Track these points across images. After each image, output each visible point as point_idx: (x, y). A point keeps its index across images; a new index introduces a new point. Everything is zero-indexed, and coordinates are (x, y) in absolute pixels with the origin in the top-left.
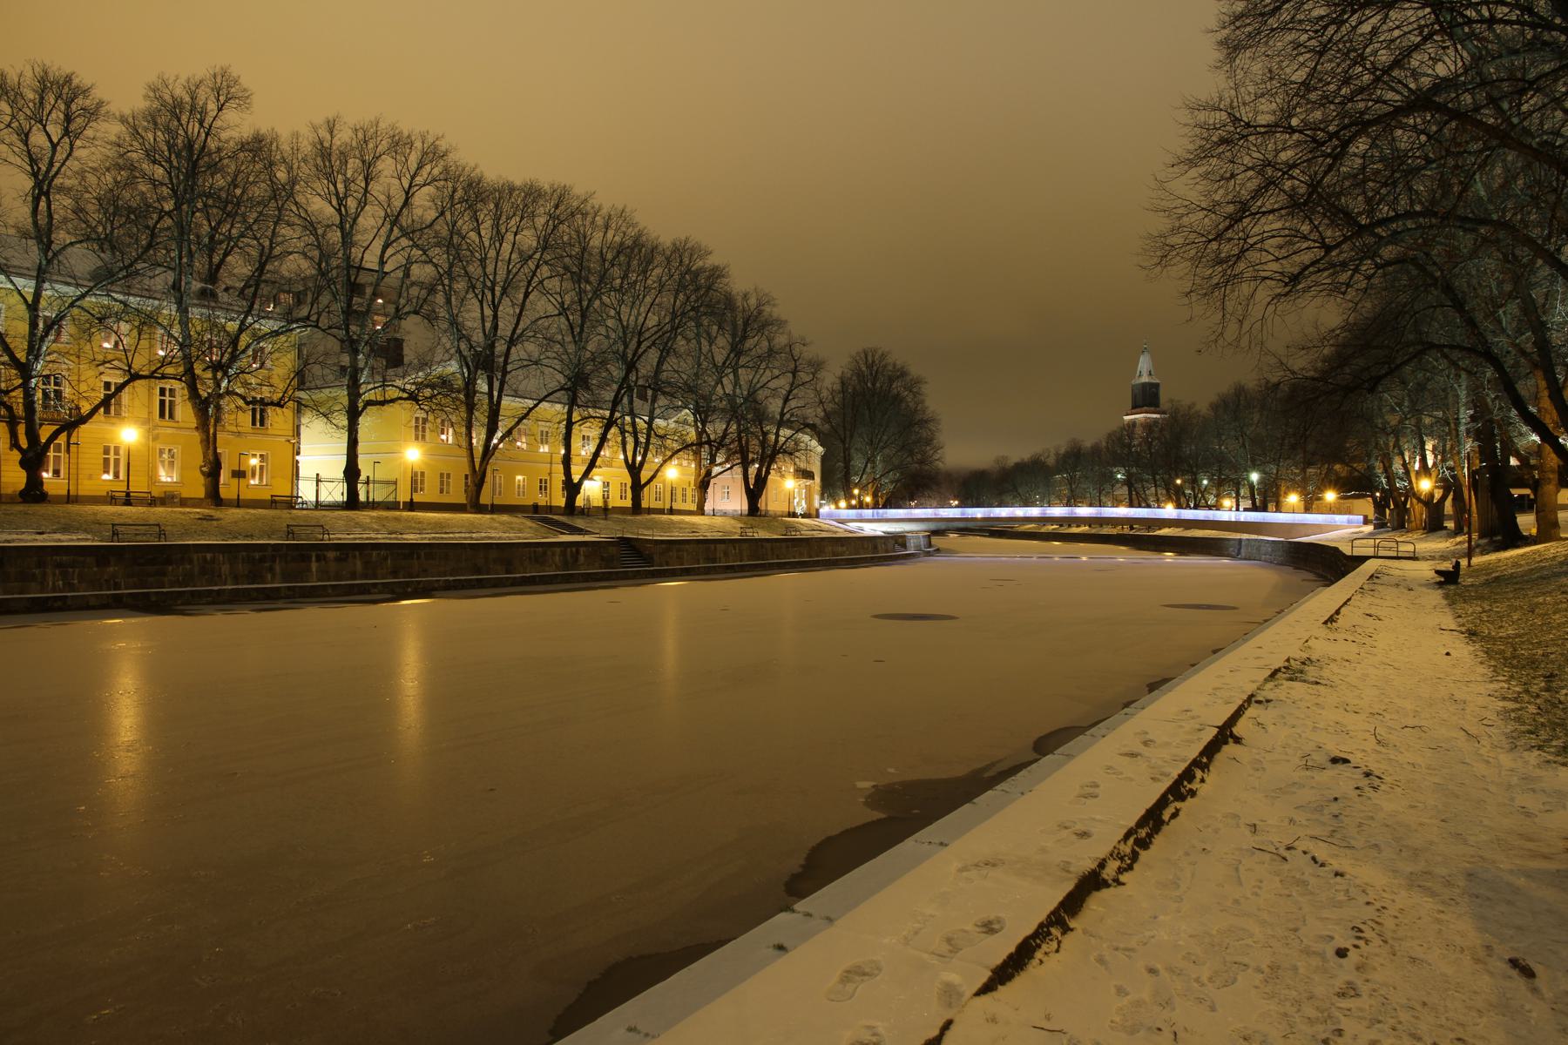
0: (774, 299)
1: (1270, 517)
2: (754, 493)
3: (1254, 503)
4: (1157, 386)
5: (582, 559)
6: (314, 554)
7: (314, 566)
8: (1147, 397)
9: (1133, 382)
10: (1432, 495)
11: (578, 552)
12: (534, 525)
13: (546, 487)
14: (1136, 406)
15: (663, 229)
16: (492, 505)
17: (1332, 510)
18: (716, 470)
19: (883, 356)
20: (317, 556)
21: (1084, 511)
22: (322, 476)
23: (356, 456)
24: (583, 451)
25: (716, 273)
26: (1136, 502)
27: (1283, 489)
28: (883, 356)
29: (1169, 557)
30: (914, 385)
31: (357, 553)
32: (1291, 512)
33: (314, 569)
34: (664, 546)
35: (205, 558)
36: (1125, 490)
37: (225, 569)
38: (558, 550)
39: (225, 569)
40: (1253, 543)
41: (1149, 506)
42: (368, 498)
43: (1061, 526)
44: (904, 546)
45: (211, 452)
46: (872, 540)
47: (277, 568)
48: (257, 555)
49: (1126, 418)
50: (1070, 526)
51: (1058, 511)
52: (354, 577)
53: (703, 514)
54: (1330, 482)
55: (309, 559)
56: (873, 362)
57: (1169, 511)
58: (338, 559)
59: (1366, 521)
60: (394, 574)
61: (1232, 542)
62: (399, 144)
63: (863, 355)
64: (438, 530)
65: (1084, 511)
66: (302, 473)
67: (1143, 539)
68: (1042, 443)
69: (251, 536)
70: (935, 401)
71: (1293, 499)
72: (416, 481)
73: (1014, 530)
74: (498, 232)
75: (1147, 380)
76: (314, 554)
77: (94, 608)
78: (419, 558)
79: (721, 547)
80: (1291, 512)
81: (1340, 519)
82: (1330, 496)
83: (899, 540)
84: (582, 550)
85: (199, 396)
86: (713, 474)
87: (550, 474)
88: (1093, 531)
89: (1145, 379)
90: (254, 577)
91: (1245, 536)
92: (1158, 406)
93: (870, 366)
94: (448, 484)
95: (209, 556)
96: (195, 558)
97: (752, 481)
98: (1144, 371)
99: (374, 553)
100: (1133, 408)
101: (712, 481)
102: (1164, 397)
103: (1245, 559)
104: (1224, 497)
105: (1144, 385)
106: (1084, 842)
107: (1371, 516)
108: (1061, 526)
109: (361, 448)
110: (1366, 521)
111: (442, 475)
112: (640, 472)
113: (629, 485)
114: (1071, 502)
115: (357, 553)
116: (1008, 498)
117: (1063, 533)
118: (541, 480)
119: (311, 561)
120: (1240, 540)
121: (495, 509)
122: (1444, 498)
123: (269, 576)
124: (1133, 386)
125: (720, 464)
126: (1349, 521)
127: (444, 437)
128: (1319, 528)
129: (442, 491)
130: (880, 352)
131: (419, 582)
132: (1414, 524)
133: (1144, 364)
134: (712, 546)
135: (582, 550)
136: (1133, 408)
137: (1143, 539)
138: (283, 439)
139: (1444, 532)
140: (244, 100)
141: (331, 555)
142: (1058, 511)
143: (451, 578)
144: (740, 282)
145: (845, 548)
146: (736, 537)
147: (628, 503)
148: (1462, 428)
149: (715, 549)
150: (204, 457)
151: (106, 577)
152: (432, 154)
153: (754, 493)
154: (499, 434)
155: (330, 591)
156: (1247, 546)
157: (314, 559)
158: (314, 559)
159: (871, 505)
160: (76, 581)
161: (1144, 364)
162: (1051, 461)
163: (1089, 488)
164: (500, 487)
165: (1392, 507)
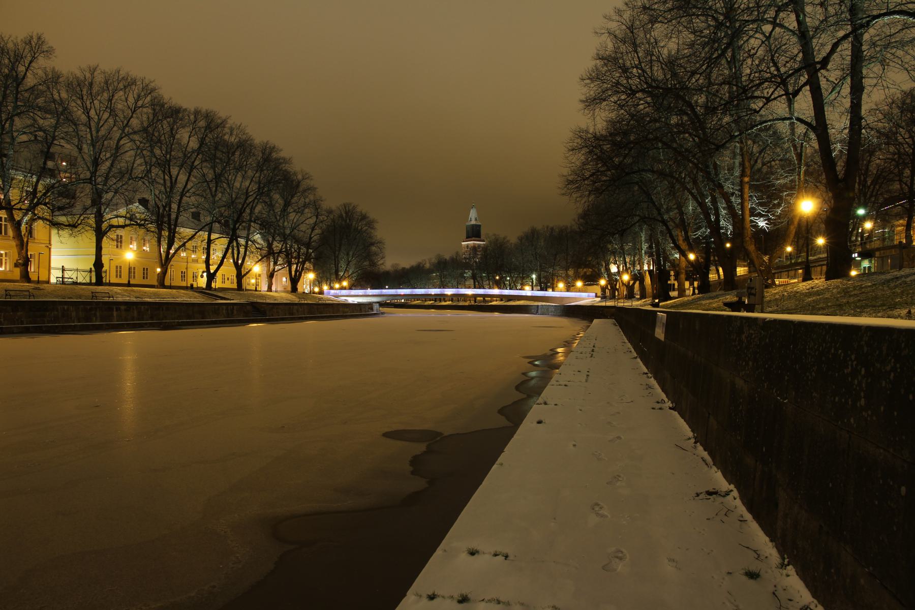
0: (311, 176)
1: (549, 293)
2: (295, 281)
3: (541, 288)
4: (479, 226)
5: (235, 312)
6: (115, 307)
7: (115, 313)
8: (474, 232)
9: (467, 224)
10: (629, 283)
11: (233, 308)
12: (199, 295)
13: (184, 276)
14: (469, 237)
15: (259, 136)
16: (171, 286)
17: (580, 291)
18: (277, 268)
19: (354, 207)
20: (116, 308)
21: (449, 292)
22: (66, 267)
23: (101, 256)
24: (216, 256)
25: (286, 161)
26: (477, 286)
27: (556, 280)
28: (354, 207)
29: (496, 314)
30: (371, 224)
31: (135, 307)
32: (559, 292)
33: (115, 315)
34: (271, 306)
35: (64, 308)
36: (472, 281)
37: (74, 314)
38: (224, 307)
39: (74, 314)
40: (545, 307)
41: (484, 288)
42: (91, 280)
43: (435, 301)
44: (372, 309)
45: (24, 251)
46: (360, 305)
47: (98, 314)
48: (88, 307)
49: (463, 243)
50: (440, 301)
51: (433, 291)
52: (133, 319)
53: (271, 291)
54: (579, 277)
55: (113, 310)
56: (349, 210)
57: (496, 291)
58: (125, 310)
59: (596, 296)
60: (152, 318)
61: (534, 307)
62: (129, 83)
63: (343, 207)
64: (157, 297)
65: (449, 292)
66: (53, 265)
67: (481, 306)
68: (427, 258)
69: (71, 298)
70: (380, 233)
71: (561, 285)
72: (131, 270)
73: (408, 304)
74: (172, 133)
75: (474, 223)
76: (115, 307)
77: (16, 333)
78: (163, 310)
79: (296, 307)
80: (559, 292)
81: (584, 295)
82: (579, 284)
83: (370, 305)
84: (235, 307)
85: (14, 220)
86: (276, 270)
87: (187, 268)
88: (454, 304)
89: (473, 222)
90: (88, 319)
91: (540, 304)
92: (480, 238)
93: (346, 213)
94: (147, 273)
95: (66, 307)
96: (59, 308)
97: (293, 273)
98: (473, 217)
99: (142, 307)
100: (467, 238)
101: (275, 273)
102: (483, 232)
103: (541, 314)
104: (525, 285)
105: (473, 225)
106: (556, 403)
107: (599, 294)
108: (435, 301)
109: (104, 251)
110: (596, 296)
111: (144, 269)
112: (241, 268)
113: (235, 275)
114: (443, 286)
115: (135, 307)
116: (400, 284)
117: (459, 304)
118: (182, 272)
119: (113, 311)
120: (538, 306)
121: (171, 287)
122: (634, 284)
123: (94, 319)
124: (467, 226)
125: (280, 265)
126: (588, 296)
127: (145, 248)
128: (575, 299)
129: (144, 278)
130: (353, 205)
131: (166, 322)
132: (620, 296)
133: (473, 214)
134: (292, 307)
135: (235, 307)
136: (467, 238)
137: (481, 306)
138: (44, 246)
139: (635, 299)
140: (49, 52)
141: (123, 307)
142: (433, 291)
143: (180, 321)
144: (297, 166)
145: (348, 309)
146: (296, 302)
147: (235, 286)
148: (643, 252)
149: (293, 308)
150: (19, 255)
151: (17, 318)
152: (148, 90)
153: (295, 281)
154: (176, 245)
155: (126, 326)
156: (541, 308)
157: (115, 310)
158: (115, 310)
159: (347, 287)
160: (2, 320)
161: (473, 214)
162: (427, 266)
163: (451, 281)
164: (173, 276)
165: (609, 288)
